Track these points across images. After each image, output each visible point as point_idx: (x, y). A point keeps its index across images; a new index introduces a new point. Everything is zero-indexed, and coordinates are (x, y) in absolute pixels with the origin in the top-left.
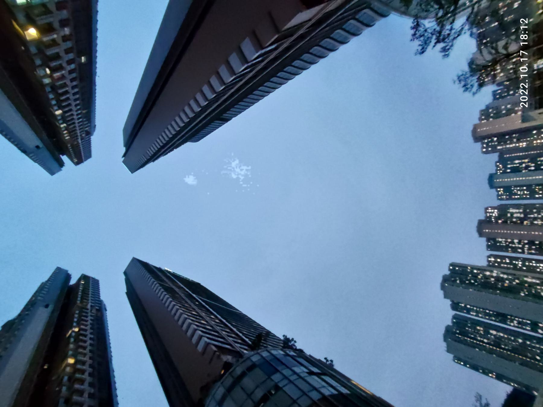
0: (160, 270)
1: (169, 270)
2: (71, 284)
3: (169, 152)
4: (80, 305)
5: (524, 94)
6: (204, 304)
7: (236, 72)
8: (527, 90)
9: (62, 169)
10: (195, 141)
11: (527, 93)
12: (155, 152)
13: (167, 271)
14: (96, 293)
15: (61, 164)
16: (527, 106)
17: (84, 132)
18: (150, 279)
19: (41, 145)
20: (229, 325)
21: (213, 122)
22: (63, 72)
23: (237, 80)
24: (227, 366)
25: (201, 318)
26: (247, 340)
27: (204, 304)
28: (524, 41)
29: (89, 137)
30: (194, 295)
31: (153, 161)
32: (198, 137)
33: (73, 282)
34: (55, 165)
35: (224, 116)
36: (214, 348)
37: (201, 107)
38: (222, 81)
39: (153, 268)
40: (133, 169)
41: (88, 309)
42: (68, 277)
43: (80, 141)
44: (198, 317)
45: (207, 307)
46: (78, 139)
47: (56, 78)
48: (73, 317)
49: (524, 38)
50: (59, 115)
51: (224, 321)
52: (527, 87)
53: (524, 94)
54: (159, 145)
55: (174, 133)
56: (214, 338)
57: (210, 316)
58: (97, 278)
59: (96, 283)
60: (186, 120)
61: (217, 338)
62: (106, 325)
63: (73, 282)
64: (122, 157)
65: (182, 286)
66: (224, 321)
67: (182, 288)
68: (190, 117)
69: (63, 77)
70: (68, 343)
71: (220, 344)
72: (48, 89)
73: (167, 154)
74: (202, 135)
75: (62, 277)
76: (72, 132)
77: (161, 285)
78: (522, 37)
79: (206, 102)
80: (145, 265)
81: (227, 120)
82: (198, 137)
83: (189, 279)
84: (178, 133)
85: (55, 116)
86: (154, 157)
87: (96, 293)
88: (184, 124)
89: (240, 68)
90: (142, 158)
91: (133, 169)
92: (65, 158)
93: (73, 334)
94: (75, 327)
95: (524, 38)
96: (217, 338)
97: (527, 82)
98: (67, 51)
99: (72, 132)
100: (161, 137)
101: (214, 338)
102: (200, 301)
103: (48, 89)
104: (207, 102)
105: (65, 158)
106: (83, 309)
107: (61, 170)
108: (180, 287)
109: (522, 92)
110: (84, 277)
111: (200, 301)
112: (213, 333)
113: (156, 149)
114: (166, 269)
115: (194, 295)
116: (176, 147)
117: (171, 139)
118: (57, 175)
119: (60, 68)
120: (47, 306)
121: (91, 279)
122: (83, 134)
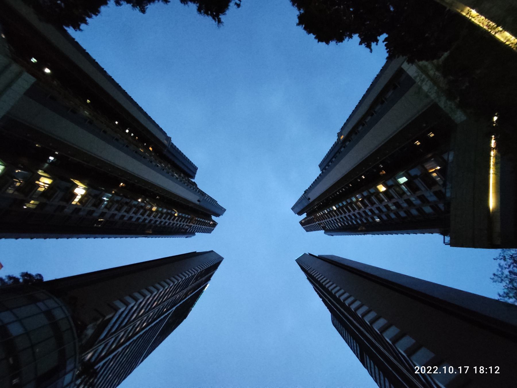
0: (209, 279)
1: (206, 288)
2: (212, 217)
3: (318, 293)
4: (194, 219)
5: (427, 370)
6: (162, 317)
7: (396, 345)
8: (437, 373)
9: (296, 214)
10: (333, 320)
11: (428, 373)
12: (316, 279)
13: (206, 286)
14: (201, 231)
15: (300, 213)
16: (416, 373)
17: (324, 225)
18: (201, 268)
19: (311, 201)
20: (128, 344)
21: (357, 342)
22: (363, 208)
23: (394, 354)
24: (82, 328)
25: (147, 310)
26: (101, 364)
27: (162, 317)
28: (478, 370)
29: (321, 228)
30: (174, 308)
31: (308, 278)
32: (335, 322)
33: (213, 218)
34: (298, 210)
35: (366, 358)
36: (108, 317)
37: (339, 297)
38: (384, 329)
39: (212, 273)
40: (299, 261)
41: (189, 223)
42: (218, 215)
43: (317, 223)
44: (149, 307)
45: (158, 321)
46: (319, 221)
47: (358, 204)
48: (186, 214)
49: (482, 370)
50: (333, 209)
51: (135, 338)
52: (434, 373)
53: (427, 370)
54: (332, 290)
55: (337, 295)
56: (121, 319)
57: (146, 321)
58: (213, 232)
59: (209, 231)
60: (342, 298)
61: (119, 322)
62: (177, 236)
63: (213, 218)
64: (310, 253)
65: (187, 298)
66: (135, 338)
67: (185, 297)
68: (351, 307)
69: (360, 208)
70: (168, 209)
71: (109, 326)
72: (349, 201)
73: (316, 291)
74: (347, 338)
75: (218, 212)
76: (322, 217)
77: (193, 276)
78: (482, 368)
79: (361, 315)
80: (215, 267)
81: (362, 361)
82: (335, 322)
83: (193, 307)
84: (343, 305)
85: (331, 206)
86: (311, 278)
87: (201, 231)
88: (338, 297)
89: (388, 337)
90: (308, 267)
91: (299, 261)
92: (304, 215)
93: (173, 213)
94: (178, 214)
95: (482, 370)
96: (119, 322)
97: (439, 373)
98: (378, 209)
99: (322, 217)
100: (328, 281)
101: (121, 319)
102: (166, 314)
103: (349, 201)
104: (360, 317)
105: (304, 215)
106: (191, 220)
107: (295, 214)
108: (186, 295)
109: (429, 368)
110: (215, 224)
111: (166, 314)
112: (126, 320)
113: (319, 280)
114: (208, 285)
115: (174, 308)
116: (324, 301)
117: (330, 293)
118: (292, 212)
119: (365, 206)
120: (199, 201)
121: (213, 228)
122: (323, 225)
